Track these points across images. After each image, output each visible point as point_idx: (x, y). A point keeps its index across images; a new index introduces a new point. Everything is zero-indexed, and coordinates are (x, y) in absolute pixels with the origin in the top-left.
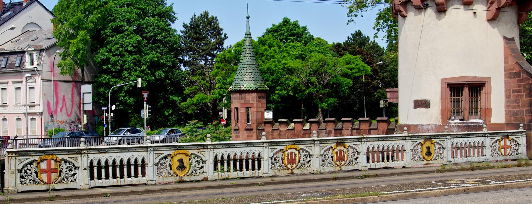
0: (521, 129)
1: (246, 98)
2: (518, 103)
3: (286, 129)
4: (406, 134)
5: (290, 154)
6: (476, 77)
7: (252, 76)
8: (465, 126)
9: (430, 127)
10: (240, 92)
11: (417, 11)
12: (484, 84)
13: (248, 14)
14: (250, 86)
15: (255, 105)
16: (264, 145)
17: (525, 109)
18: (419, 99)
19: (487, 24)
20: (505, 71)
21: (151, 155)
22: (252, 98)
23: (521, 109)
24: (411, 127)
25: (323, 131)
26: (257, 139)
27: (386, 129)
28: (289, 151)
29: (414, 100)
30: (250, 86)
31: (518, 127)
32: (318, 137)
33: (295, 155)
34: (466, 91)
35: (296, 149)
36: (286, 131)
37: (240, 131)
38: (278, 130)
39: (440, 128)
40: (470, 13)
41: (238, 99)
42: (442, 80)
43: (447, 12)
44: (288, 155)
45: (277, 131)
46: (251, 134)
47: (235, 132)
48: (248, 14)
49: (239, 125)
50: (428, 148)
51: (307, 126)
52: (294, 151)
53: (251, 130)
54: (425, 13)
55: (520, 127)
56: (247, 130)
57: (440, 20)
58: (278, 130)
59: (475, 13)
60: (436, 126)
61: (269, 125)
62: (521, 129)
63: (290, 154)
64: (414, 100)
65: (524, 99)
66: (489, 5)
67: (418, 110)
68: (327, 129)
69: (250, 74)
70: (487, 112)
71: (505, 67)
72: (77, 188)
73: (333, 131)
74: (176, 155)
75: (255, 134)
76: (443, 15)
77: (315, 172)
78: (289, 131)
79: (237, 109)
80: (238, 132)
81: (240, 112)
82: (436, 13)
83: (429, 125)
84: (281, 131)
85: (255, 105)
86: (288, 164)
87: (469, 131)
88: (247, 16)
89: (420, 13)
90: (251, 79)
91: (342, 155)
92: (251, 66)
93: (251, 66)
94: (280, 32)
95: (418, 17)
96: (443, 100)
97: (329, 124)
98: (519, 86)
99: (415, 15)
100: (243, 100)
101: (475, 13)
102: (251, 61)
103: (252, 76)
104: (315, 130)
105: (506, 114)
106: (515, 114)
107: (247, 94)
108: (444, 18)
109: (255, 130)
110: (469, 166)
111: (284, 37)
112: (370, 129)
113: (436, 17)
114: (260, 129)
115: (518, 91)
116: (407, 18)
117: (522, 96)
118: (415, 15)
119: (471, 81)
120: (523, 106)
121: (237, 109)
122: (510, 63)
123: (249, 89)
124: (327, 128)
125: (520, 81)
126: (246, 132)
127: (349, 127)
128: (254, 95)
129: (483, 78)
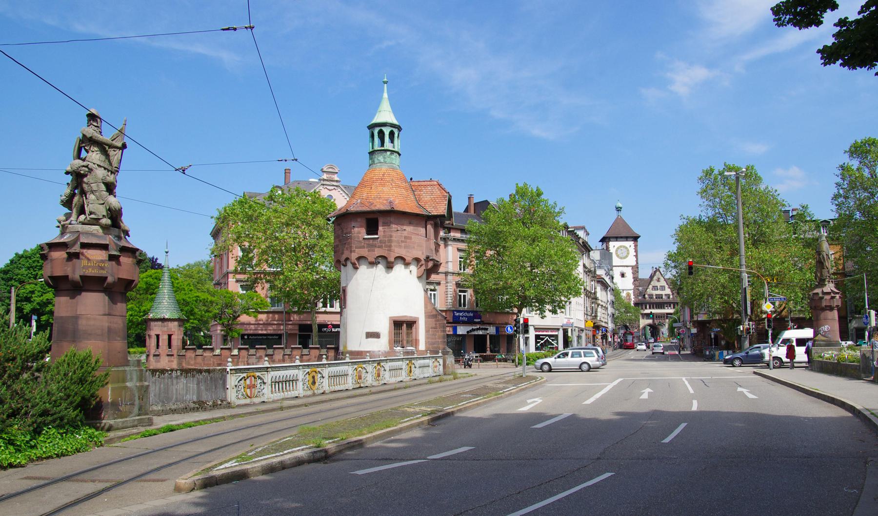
0: (440, 354)
1: (168, 326)
2: (435, 336)
3: (211, 355)
4: (368, 359)
6: (411, 317)
7: (173, 306)
8: (405, 352)
9: (380, 353)
10: (163, 320)
11: (370, 266)
12: (415, 322)
13: (167, 248)
14: (173, 315)
15: (176, 333)
16: (350, 364)
19: (416, 279)
20: (425, 313)
21: (370, 366)
22: (174, 326)
23: (437, 340)
24: (363, 353)
25: (253, 356)
26: (335, 360)
27: (318, 354)
29: (366, 333)
30: (173, 315)
31: (438, 353)
32: (371, 358)
34: (405, 325)
36: (211, 357)
37: (162, 357)
38: (202, 355)
39: (386, 354)
40: (408, 271)
41: (159, 327)
42: (390, 318)
43: (393, 269)
45: (201, 356)
46: (172, 359)
47: (154, 357)
48: (167, 248)
49: (160, 350)
51: (235, 352)
53: (173, 355)
54: (376, 267)
55: (323, 358)
56: (168, 355)
57: (388, 273)
58: (202, 355)
59: (411, 271)
60: (385, 352)
61: (192, 351)
62: (440, 354)
64: (366, 333)
65: (440, 333)
66: (419, 266)
67: (370, 340)
68: (258, 355)
69: (172, 304)
70: (416, 343)
71: (425, 310)
72: (266, 401)
75: (176, 359)
76: (390, 270)
77: (370, 385)
78: (215, 357)
79: (158, 336)
80: (158, 357)
81: (162, 339)
82: (385, 268)
83: (379, 351)
84: (205, 357)
85: (176, 333)
87: (408, 356)
88: (167, 250)
89: (372, 267)
90: (173, 309)
92: (171, 296)
93: (171, 296)
94: (34, 259)
95: (371, 270)
96: (390, 332)
97: (259, 350)
99: (367, 268)
100: (166, 328)
101: (411, 271)
102: (171, 292)
103: (173, 306)
104: (298, 356)
105: (426, 344)
106: (433, 344)
107: (169, 322)
108: (391, 272)
109: (175, 356)
110: (426, 381)
111: (39, 264)
112: (303, 355)
113: (386, 272)
114: (181, 354)
116: (359, 271)
117: (438, 332)
118: (367, 268)
119: (409, 319)
120: (439, 338)
121: (158, 336)
122: (429, 308)
123: (172, 317)
124: (257, 353)
125: (437, 321)
126: (167, 357)
128: (176, 323)
129: (415, 317)
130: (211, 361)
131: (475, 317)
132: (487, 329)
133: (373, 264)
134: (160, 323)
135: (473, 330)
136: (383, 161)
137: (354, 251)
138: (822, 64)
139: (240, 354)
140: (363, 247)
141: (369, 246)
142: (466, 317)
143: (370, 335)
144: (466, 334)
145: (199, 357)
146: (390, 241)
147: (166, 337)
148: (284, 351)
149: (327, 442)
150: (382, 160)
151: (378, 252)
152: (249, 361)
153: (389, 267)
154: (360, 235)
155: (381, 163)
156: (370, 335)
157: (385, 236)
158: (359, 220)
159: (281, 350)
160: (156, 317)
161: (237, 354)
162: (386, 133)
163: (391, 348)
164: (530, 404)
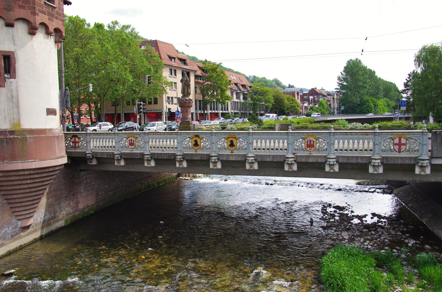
5: (309, 141)
11: (46, 35)
18: (50, 108)
24: (47, 131)
28: (130, 138)
29: (47, 109)
33: (134, 140)
35: (134, 138)
44: (308, 141)
52: (133, 138)
63: (309, 141)
74: (228, 138)
86: (307, 147)
91: (312, 143)
95: (46, 40)
133: (48, 33)
137: (38, 14)
153: (32, 32)
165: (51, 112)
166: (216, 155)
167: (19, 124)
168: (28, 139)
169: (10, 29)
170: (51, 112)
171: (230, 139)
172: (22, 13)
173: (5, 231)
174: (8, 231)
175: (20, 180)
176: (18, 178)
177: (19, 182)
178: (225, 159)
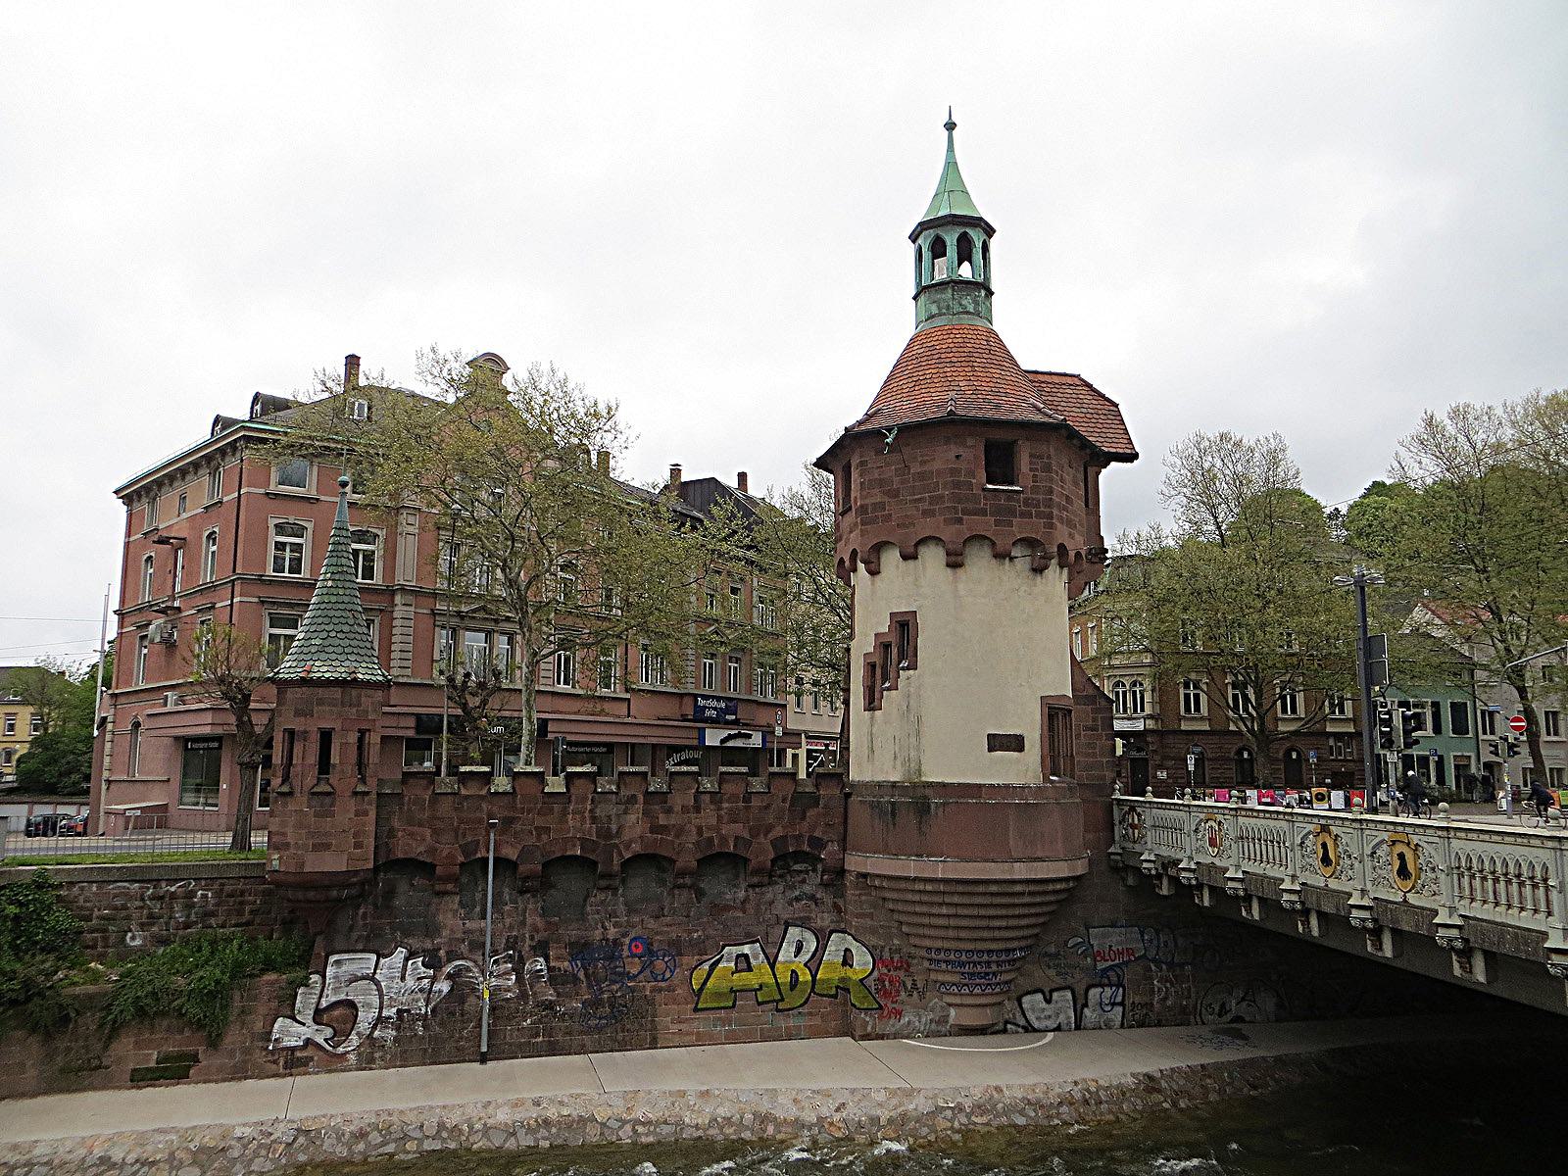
1: (359, 705)
17: (1104, 760)
49: (333, 778)
50: (1401, 856)
73: (641, 798)
79: (326, 737)
80: (328, 800)
98: (1094, 720)
100: (354, 710)
115: (1093, 729)
121: (326, 737)
127: (690, 788)
130: (482, 810)
131: (727, 711)
132: (749, 736)
133: (1001, 556)
134: (337, 693)
135: (730, 737)
136: (972, 310)
138: (742, 477)
139: (572, 790)
140: (983, 512)
141: (998, 511)
142: (715, 709)
143: (997, 743)
144: (718, 744)
145: (444, 797)
146: (1049, 503)
147: (353, 738)
148: (595, 783)
149: (111, 886)
150: (971, 308)
151: (1019, 528)
152: (598, 811)
154: (974, 481)
155: (968, 313)
156: (997, 743)
157: (1035, 489)
158: (970, 442)
159: (688, 779)
160: (327, 675)
161: (509, 788)
162: (948, 243)
163: (1046, 779)
164: (138, 808)
165: (1016, 743)
166: (1366, 902)
167: (919, 772)
168: (933, 806)
169: (911, 563)
170: (1016, 743)
171: (1399, 848)
172: (927, 527)
173: (909, 1022)
174: (917, 1024)
175: (921, 903)
176: (917, 898)
177: (924, 909)
178: (1328, 908)
